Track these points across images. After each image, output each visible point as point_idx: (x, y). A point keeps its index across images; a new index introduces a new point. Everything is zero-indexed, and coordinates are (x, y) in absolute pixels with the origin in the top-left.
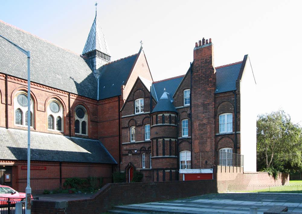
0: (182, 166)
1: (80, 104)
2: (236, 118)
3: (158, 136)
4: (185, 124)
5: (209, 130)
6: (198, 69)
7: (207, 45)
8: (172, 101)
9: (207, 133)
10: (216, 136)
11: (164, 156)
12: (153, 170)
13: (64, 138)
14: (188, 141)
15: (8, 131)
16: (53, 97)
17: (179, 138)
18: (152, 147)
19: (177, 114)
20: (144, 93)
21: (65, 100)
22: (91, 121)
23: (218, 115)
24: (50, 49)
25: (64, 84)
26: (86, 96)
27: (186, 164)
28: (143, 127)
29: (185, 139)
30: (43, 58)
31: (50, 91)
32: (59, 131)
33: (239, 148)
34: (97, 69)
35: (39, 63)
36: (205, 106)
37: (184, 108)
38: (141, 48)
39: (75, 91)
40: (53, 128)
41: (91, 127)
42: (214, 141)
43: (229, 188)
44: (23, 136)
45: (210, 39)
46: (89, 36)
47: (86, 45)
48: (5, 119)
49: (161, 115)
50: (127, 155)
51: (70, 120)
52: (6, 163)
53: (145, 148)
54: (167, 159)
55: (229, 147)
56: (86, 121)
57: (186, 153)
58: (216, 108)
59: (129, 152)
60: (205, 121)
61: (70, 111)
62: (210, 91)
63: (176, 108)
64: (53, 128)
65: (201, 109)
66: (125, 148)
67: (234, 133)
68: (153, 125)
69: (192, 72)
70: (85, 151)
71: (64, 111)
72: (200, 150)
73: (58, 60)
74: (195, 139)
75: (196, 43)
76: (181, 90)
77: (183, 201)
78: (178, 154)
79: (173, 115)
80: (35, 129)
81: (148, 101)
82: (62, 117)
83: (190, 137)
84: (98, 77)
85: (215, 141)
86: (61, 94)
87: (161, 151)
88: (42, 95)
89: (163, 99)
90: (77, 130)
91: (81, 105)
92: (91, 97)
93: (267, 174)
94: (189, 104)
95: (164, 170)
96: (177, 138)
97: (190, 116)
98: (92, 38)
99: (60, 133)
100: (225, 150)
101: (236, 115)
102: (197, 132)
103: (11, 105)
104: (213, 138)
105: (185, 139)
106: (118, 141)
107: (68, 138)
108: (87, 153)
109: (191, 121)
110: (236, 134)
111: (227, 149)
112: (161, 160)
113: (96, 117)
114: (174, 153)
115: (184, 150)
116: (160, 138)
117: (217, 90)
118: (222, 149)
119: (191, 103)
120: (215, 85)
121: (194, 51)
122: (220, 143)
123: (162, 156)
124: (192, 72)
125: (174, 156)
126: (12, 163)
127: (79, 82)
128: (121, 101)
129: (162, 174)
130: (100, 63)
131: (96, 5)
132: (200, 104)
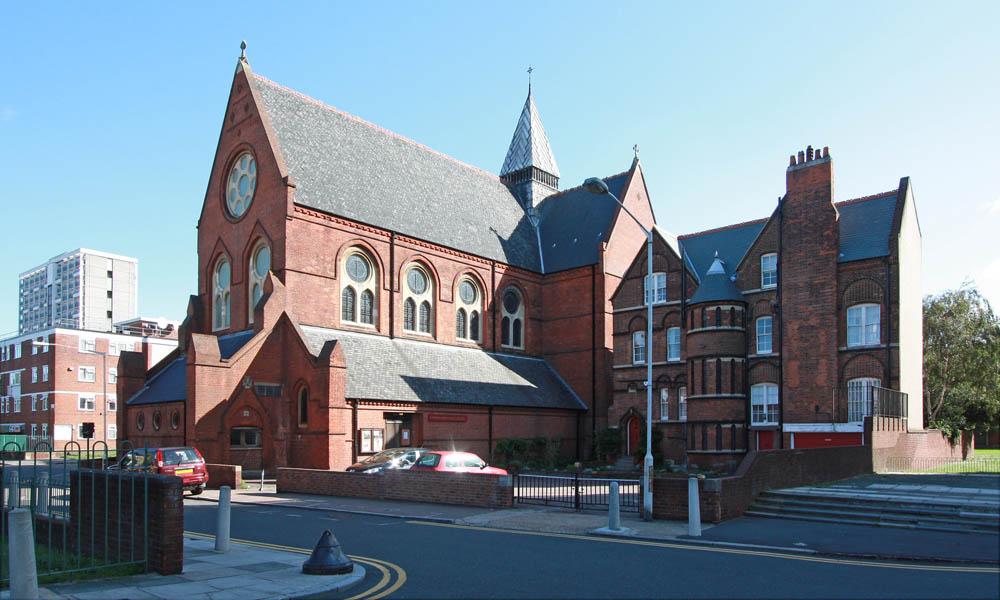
0: (755, 416)
1: (512, 284)
2: (889, 313)
3: (705, 353)
4: (763, 327)
5: (823, 339)
6: (797, 212)
7: (819, 162)
8: (733, 278)
9: (819, 347)
10: (840, 353)
11: (719, 395)
12: (691, 423)
13: (484, 355)
14: (772, 364)
15: (394, 344)
16: (352, 243)
17: (750, 356)
18: (690, 373)
19: (746, 305)
20: (668, 262)
21: (486, 276)
22: (530, 317)
23: (844, 307)
24: (449, 172)
25: (483, 244)
26: (522, 266)
27: (765, 411)
28: (662, 333)
29: (765, 358)
30: (442, 192)
31: (462, 260)
32: (474, 342)
33: (897, 378)
34: (534, 206)
35: (438, 203)
36: (814, 289)
37: (762, 292)
38: (636, 161)
39: (502, 257)
40: (464, 336)
41: (529, 330)
42: (835, 363)
43: (889, 464)
44: (419, 354)
45: (826, 149)
46: (515, 137)
47: (509, 157)
48: (388, 319)
49: (714, 308)
50: (626, 391)
51: (494, 318)
52: (406, 408)
53: (669, 378)
54: (727, 401)
55: (872, 377)
56: (522, 319)
57: (767, 387)
58: (840, 293)
59: (629, 386)
60: (813, 321)
61: (493, 298)
62: (827, 258)
63: (743, 293)
64: (464, 336)
65: (804, 295)
66: (620, 376)
67: (884, 346)
68: (694, 330)
69: (782, 217)
70: (525, 383)
71: (483, 299)
72: (801, 382)
73: (467, 194)
74: (790, 360)
75: (793, 158)
76: (756, 255)
77: (587, 491)
78: (747, 391)
79: (738, 308)
80: (435, 337)
81: (676, 278)
82: (479, 312)
83: (777, 354)
84: (536, 223)
85: (838, 364)
86: (373, 235)
87: (712, 384)
88: (447, 269)
89: (714, 275)
90: (505, 340)
91: (515, 285)
92: (531, 269)
93: (941, 435)
94: (775, 285)
95: (719, 423)
96: (744, 356)
97: (777, 310)
98: (521, 142)
99: (476, 346)
100: (861, 383)
101: (890, 309)
102: (795, 344)
103: (398, 292)
104: (834, 356)
105: (764, 357)
106: (590, 361)
107: (491, 356)
108: (529, 387)
109: (781, 320)
110: (889, 349)
111: (867, 379)
112: (712, 403)
113: (539, 309)
114: (740, 388)
115: (761, 382)
116: (712, 356)
117: (842, 255)
118: (854, 380)
119: (779, 281)
120: (837, 245)
121: (789, 174)
122: (849, 366)
123: (715, 395)
124: (782, 217)
125: (740, 395)
126: (414, 409)
127: (506, 236)
128: (597, 276)
129: (715, 433)
130: (539, 193)
131: (530, 70)
132: (801, 285)
